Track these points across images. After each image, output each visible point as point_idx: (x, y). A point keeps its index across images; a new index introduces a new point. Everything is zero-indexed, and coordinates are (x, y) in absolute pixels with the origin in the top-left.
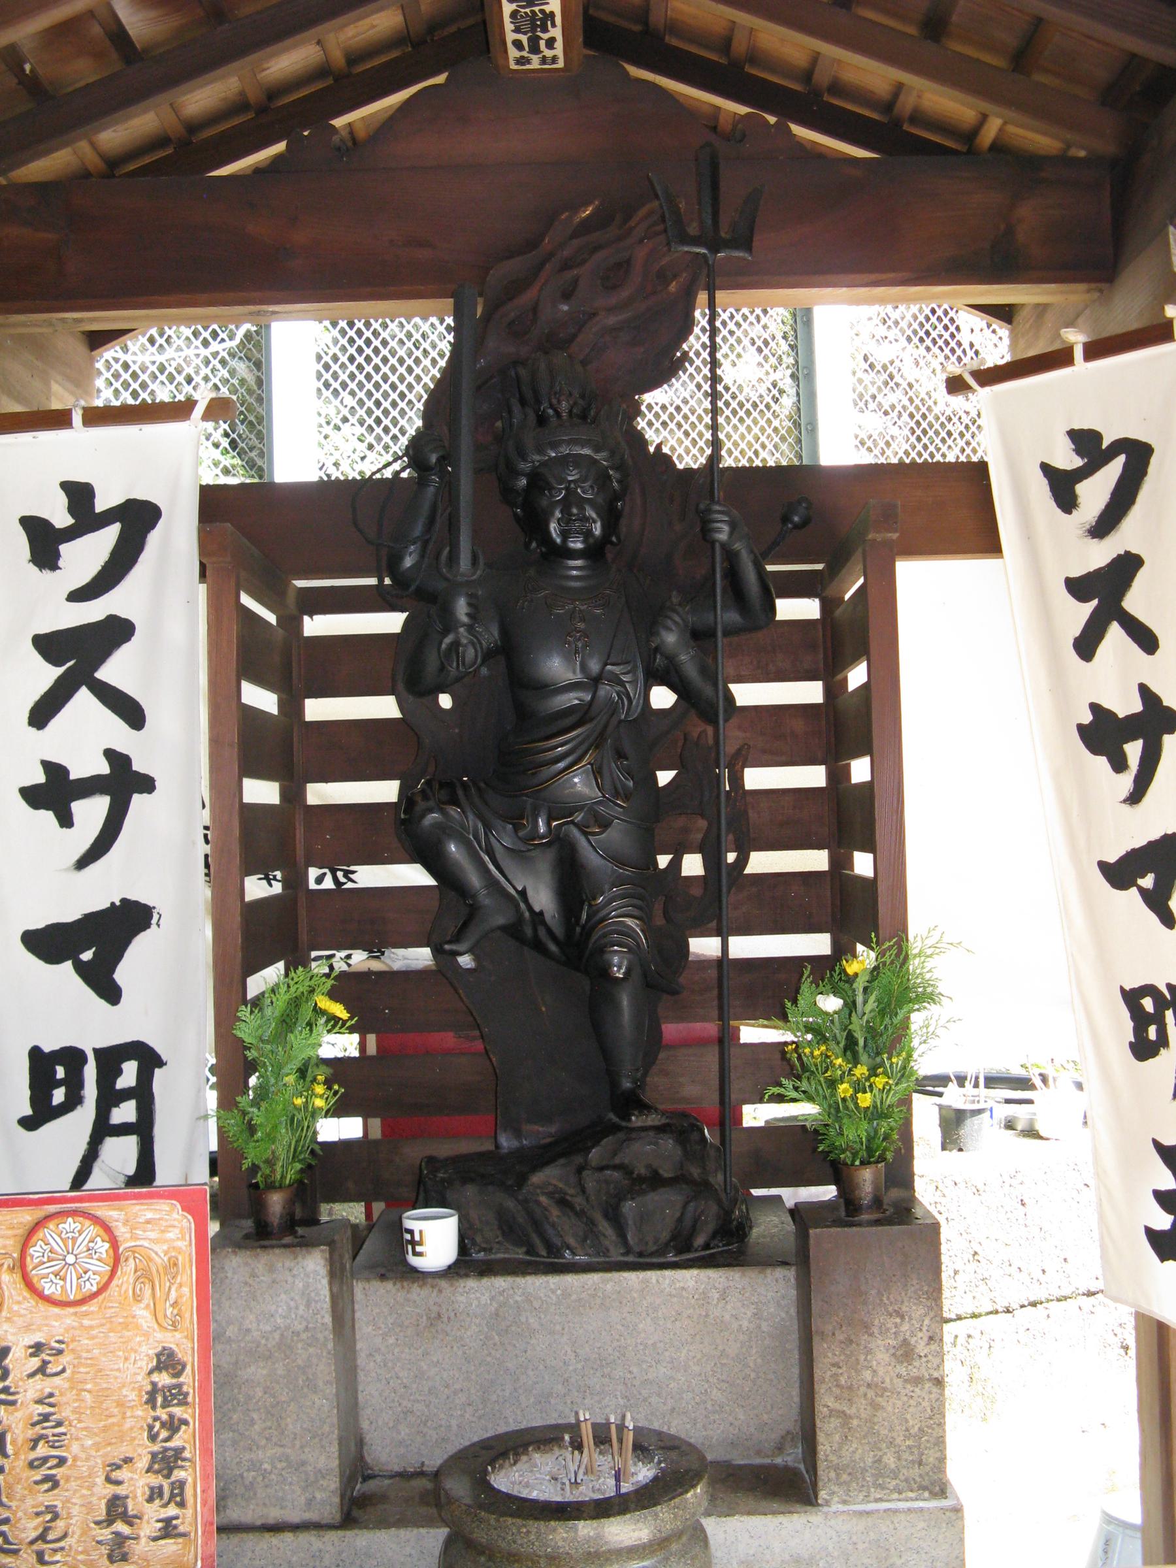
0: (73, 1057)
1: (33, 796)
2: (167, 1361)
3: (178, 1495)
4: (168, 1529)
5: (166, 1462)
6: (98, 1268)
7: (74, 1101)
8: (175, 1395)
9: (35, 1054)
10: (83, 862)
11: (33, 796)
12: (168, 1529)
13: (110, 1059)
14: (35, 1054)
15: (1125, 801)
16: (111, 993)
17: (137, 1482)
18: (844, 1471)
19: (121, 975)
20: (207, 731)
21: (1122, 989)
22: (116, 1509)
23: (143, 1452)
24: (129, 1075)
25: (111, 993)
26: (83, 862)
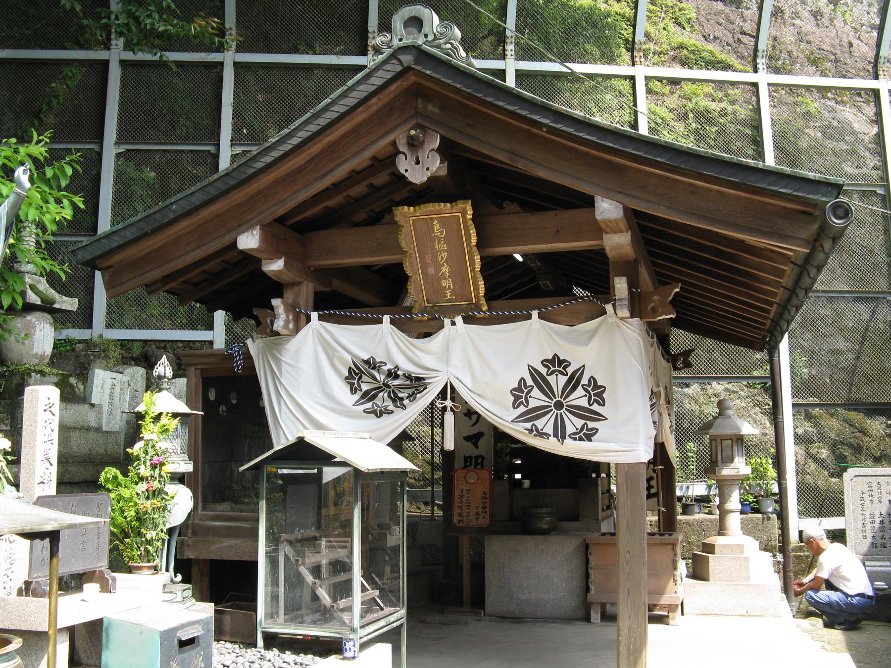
0: (471, 457)
1: (465, 415)
2: (485, 493)
3: (486, 512)
4: (484, 517)
5: (484, 508)
6: (476, 479)
7: (471, 464)
8: (486, 498)
9: (465, 457)
10: (473, 425)
11: (465, 415)
12: (484, 517)
13: (477, 458)
14: (465, 457)
15: (846, 545)
16: (477, 447)
17: (480, 510)
18: (749, 455)
19: (479, 444)
20: (550, 179)
21: (838, 568)
22: (477, 513)
23: (481, 506)
24: (480, 461)
25: (477, 447)
26: (473, 425)
